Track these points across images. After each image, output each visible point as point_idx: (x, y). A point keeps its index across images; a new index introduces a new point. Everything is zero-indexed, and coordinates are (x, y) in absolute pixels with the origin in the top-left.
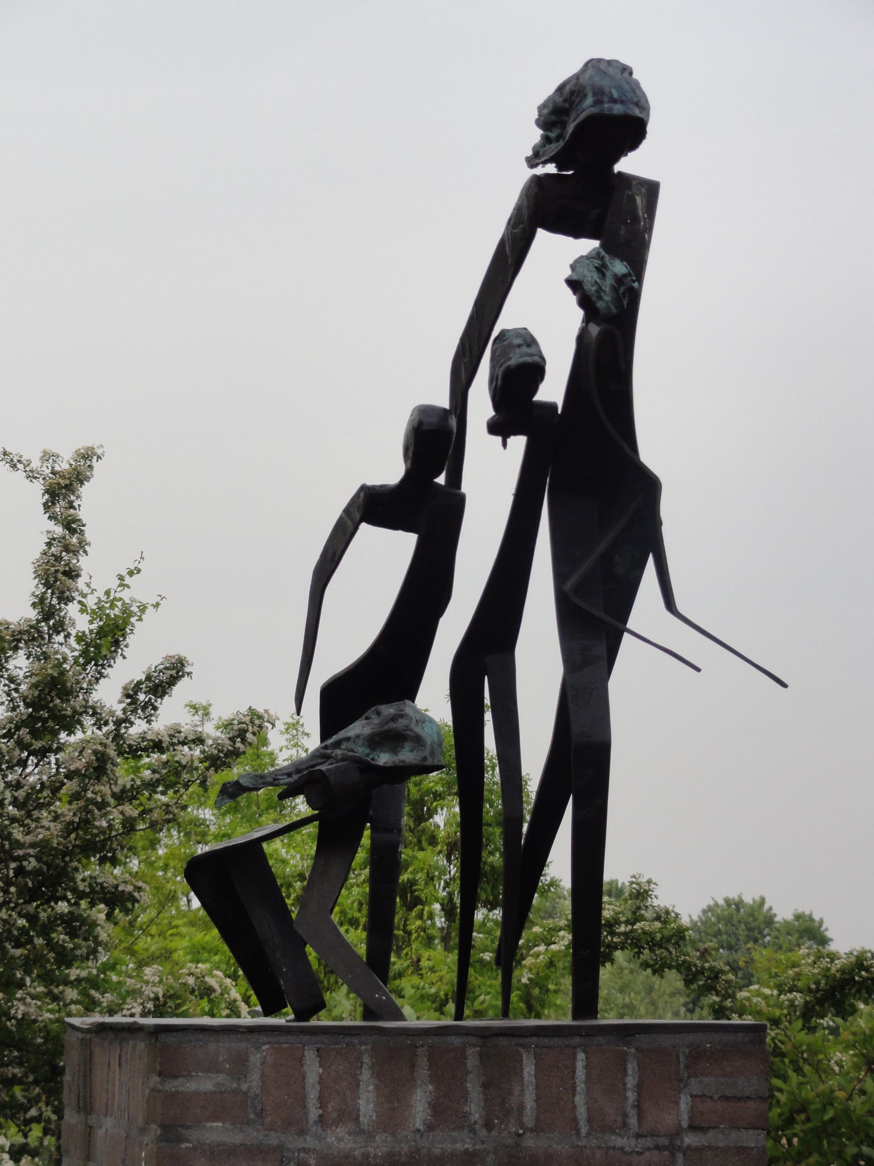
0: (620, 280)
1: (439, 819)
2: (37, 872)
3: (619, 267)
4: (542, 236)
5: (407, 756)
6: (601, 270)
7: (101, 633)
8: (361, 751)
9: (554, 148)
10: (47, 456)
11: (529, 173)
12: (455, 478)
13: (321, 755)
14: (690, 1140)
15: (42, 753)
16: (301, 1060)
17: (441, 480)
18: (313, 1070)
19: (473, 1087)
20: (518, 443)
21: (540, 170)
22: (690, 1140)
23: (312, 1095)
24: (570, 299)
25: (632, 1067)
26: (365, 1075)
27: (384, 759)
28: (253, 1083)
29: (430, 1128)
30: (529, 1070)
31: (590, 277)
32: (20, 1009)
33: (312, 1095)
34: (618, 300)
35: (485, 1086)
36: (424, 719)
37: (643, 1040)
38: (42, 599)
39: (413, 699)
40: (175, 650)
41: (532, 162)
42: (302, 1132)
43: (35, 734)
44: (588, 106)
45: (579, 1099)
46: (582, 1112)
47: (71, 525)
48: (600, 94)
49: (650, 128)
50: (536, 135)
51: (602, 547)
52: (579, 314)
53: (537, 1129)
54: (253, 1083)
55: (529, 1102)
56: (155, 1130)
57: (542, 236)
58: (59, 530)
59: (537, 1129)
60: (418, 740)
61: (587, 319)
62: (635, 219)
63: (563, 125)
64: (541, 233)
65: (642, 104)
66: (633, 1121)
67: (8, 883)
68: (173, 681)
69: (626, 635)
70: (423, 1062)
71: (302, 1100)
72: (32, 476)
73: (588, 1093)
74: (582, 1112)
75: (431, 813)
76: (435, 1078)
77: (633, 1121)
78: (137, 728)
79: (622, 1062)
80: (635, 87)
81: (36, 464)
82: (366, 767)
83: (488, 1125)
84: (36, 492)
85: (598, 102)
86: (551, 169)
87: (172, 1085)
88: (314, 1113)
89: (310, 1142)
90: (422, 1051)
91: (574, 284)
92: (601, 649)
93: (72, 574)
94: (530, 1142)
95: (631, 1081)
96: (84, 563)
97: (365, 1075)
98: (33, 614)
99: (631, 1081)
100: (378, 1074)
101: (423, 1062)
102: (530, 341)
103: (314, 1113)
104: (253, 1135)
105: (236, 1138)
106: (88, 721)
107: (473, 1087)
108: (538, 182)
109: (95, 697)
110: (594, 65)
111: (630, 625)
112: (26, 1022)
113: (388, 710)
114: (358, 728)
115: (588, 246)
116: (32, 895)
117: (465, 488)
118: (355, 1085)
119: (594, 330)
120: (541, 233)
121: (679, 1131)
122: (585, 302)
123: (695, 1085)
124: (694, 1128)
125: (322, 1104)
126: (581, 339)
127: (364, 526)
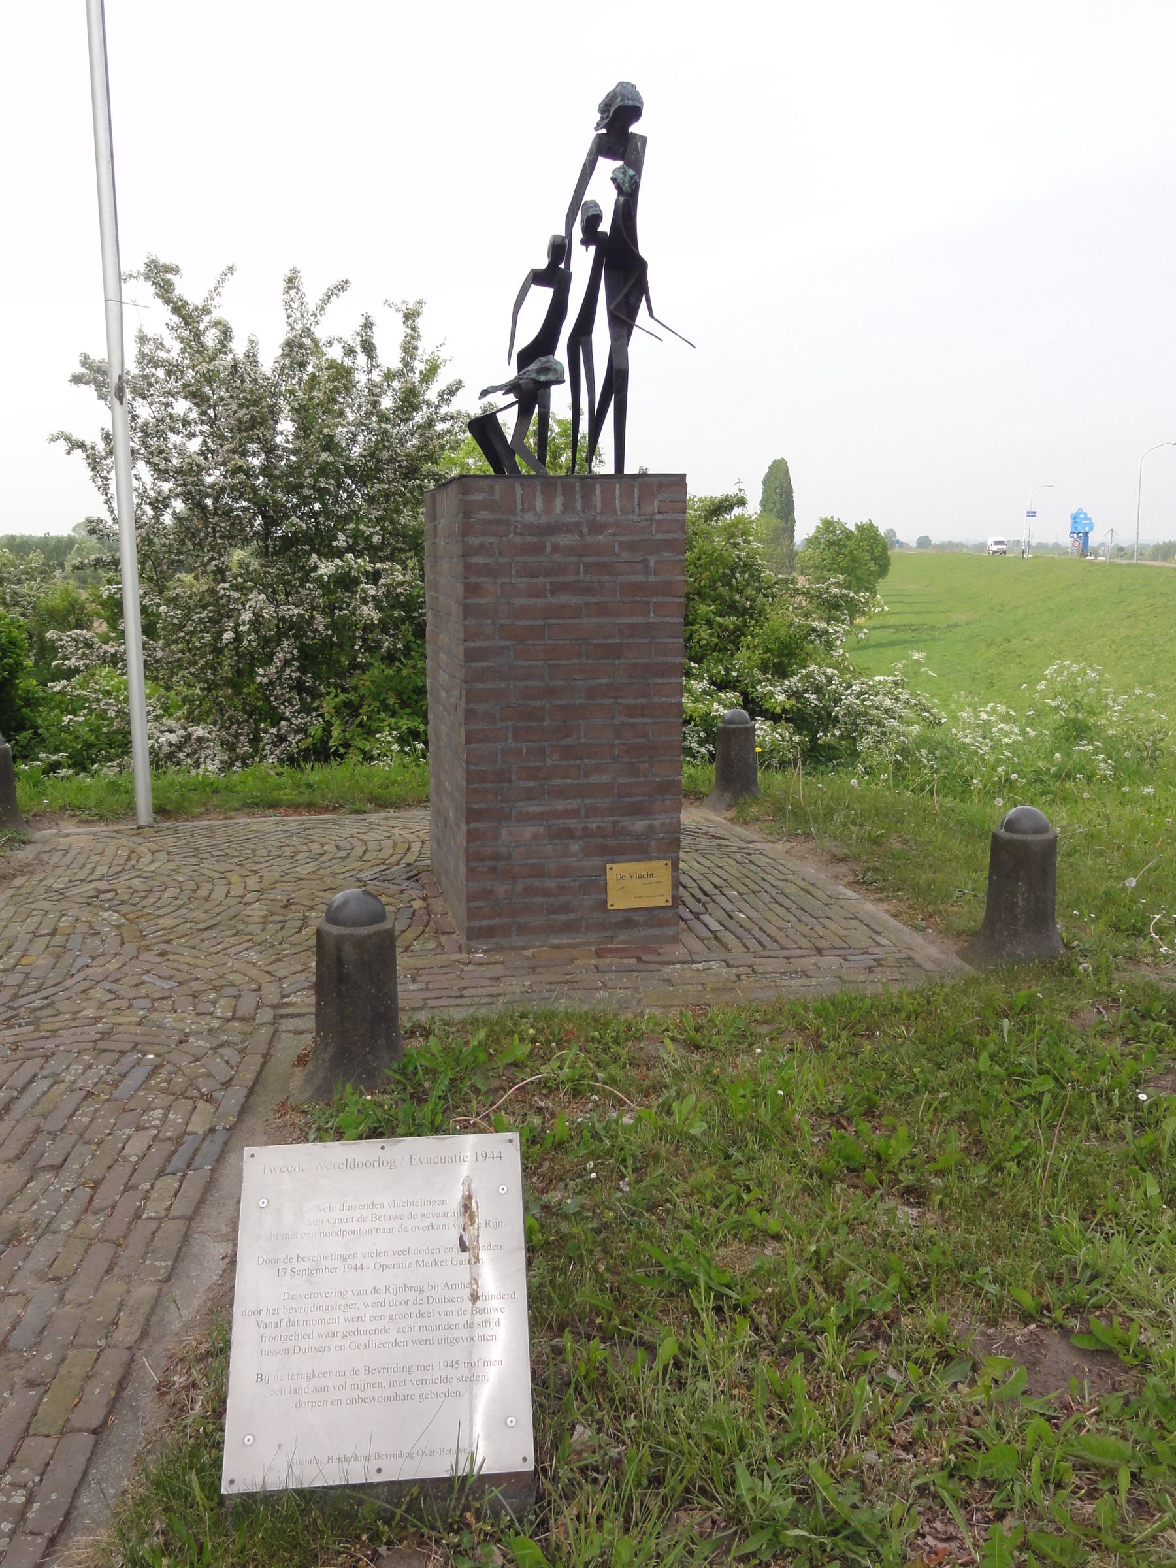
0: (632, 177)
1: (563, 458)
2: (407, 467)
3: (631, 172)
4: (601, 159)
5: (551, 377)
6: (624, 173)
7: (429, 371)
8: (534, 376)
9: (605, 122)
10: (404, 302)
11: (594, 134)
12: (568, 265)
13: (518, 378)
14: (658, 517)
15: (406, 420)
16: (514, 488)
17: (562, 266)
18: (519, 492)
19: (578, 497)
20: (592, 248)
21: (601, 131)
22: (658, 517)
23: (519, 501)
24: (612, 186)
25: (636, 490)
26: (538, 493)
27: (542, 378)
28: (497, 496)
29: (563, 513)
30: (598, 491)
31: (620, 176)
32: (403, 521)
33: (519, 501)
34: (631, 187)
35: (583, 497)
36: (557, 363)
37: (640, 480)
38: (404, 359)
39: (553, 354)
40: (457, 377)
41: (596, 129)
42: (515, 515)
43: (404, 413)
44: (618, 102)
45: (617, 502)
46: (618, 507)
47: (414, 329)
48: (623, 96)
49: (644, 112)
50: (598, 117)
51: (626, 290)
52: (616, 192)
53: (602, 513)
54: (497, 496)
55: (599, 504)
56: (461, 515)
57: (601, 159)
58: (409, 331)
59: (602, 513)
60: (555, 370)
61: (619, 195)
62: (638, 153)
63: (609, 111)
64: (600, 158)
65: (640, 100)
66: (637, 510)
67: (396, 470)
68: (457, 389)
69: (630, 468)
70: (559, 488)
71: (515, 502)
72: (398, 310)
73: (621, 500)
74: (618, 507)
75: (560, 455)
76: (563, 494)
77: (637, 510)
78: (444, 410)
79: (632, 487)
80: (637, 93)
81: (399, 305)
82: (536, 382)
83: (584, 511)
84: (400, 317)
85: (622, 100)
86: (604, 131)
87: (467, 498)
88: (519, 508)
89: (518, 518)
90: (559, 484)
91: (614, 180)
92: (625, 332)
93: (416, 348)
94: (599, 518)
95: (636, 495)
96: (420, 344)
97: (538, 493)
98: (401, 366)
99: (636, 495)
100: (543, 492)
101: (559, 488)
102: (597, 205)
103: (519, 508)
104: (497, 516)
105: (490, 517)
106: (424, 407)
107: (578, 497)
108: (599, 136)
109: (426, 397)
110: (621, 84)
111: (637, 322)
112: (405, 526)
113: (543, 359)
114: (533, 367)
115: (619, 164)
116: (405, 476)
117: (572, 269)
118: (535, 496)
119: (622, 199)
120: (600, 158)
121: (654, 514)
122: (618, 187)
123: (660, 497)
124: (659, 512)
125: (522, 505)
126: (616, 203)
127: (533, 286)
